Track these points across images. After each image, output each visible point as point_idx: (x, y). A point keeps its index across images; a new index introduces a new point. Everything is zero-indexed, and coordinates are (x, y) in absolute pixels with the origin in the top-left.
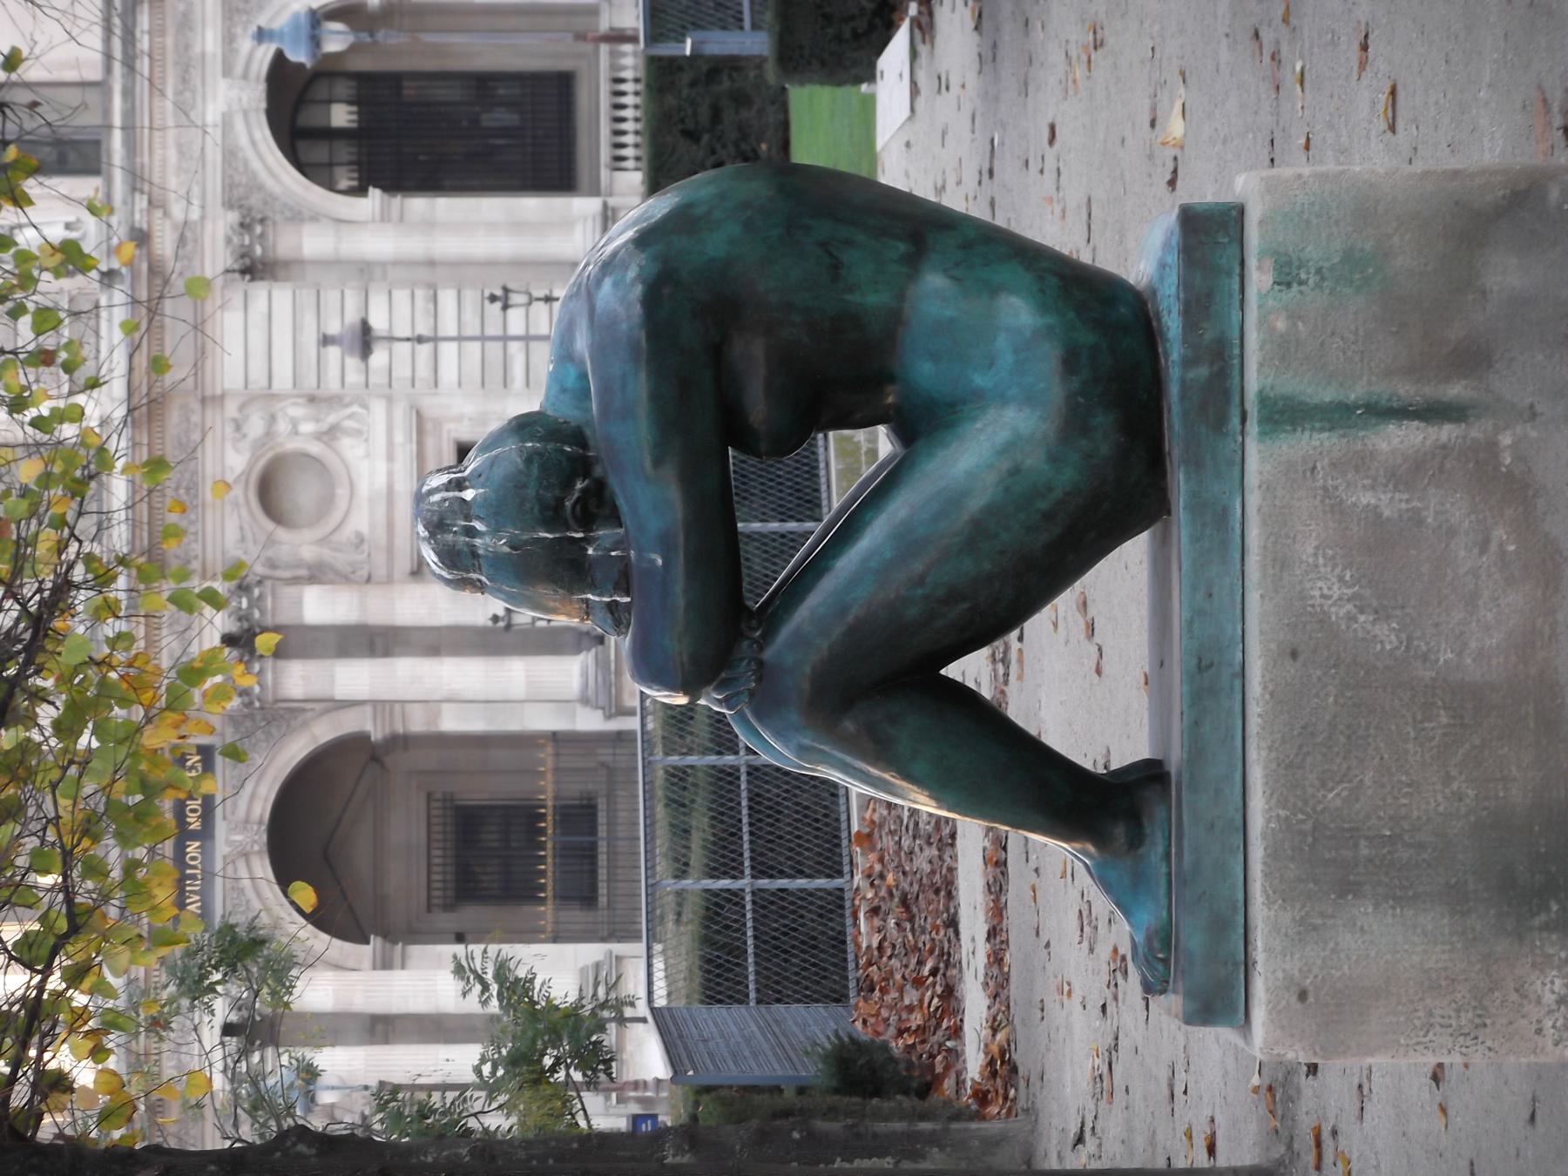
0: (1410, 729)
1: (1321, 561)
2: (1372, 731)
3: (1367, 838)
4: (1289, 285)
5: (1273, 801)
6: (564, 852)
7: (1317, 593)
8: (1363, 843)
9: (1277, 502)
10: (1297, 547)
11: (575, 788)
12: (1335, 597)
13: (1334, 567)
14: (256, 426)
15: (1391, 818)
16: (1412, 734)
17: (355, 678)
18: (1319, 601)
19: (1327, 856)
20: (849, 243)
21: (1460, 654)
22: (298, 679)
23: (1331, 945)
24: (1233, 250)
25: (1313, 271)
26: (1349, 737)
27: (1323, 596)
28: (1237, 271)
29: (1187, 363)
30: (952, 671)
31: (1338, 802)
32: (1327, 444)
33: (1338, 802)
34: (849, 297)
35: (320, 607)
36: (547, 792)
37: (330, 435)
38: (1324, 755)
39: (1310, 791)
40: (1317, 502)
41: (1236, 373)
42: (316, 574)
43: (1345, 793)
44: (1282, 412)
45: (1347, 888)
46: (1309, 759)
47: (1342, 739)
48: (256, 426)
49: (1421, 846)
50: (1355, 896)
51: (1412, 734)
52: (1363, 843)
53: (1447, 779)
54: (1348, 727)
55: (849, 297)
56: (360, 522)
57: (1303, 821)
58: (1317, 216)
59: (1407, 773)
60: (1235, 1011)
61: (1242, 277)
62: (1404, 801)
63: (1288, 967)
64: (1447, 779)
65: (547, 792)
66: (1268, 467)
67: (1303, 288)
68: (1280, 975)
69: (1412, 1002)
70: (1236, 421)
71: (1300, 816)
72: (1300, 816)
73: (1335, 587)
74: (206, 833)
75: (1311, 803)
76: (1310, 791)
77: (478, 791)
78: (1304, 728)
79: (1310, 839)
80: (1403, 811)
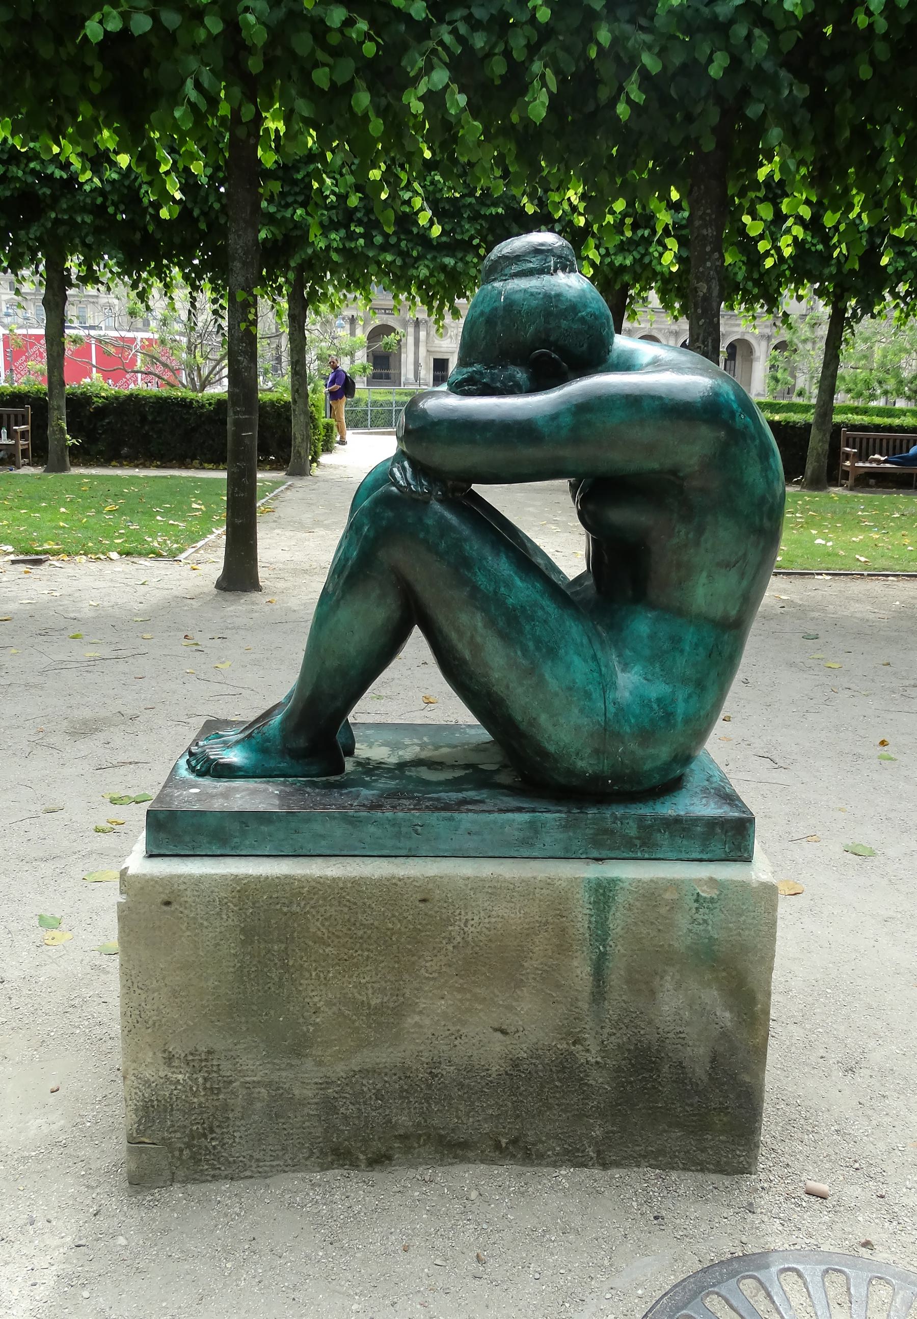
0: (367, 979)
1: (493, 920)
2: (366, 953)
3: (286, 948)
4: (696, 901)
5: (313, 884)
6: (381, 374)
7: (469, 917)
8: (283, 946)
9: (537, 890)
10: (505, 904)
11: (392, 376)
12: (466, 929)
13: (489, 929)
14: (453, 325)
15: (301, 966)
16: (363, 981)
17: (411, 340)
18: (464, 918)
19: (273, 921)
20: (742, 575)
21: (421, 1013)
22: (411, 330)
23: (205, 923)
24: (720, 853)
25: (706, 917)
26: (361, 938)
27: (467, 920)
28: (705, 857)
29: (641, 819)
30: (416, 631)
31: (313, 930)
32: (579, 925)
33: (313, 930)
34: (704, 574)
35: (423, 334)
36: (392, 371)
37: (451, 337)
38: (349, 920)
39: (322, 910)
40: (537, 918)
41: (631, 855)
42: (428, 334)
43: (319, 933)
44: (604, 894)
45: (248, 934)
46: (346, 910)
47: (360, 933)
48: (453, 325)
49: (281, 986)
50: (242, 941)
51: (363, 981)
52: (283, 946)
53: (330, 1004)
54: (369, 937)
55: (704, 574)
56: (436, 342)
57: (299, 905)
58: (744, 921)
59: (334, 977)
60: (158, 847)
61: (701, 860)
62: (314, 974)
63: (189, 893)
64: (330, 1004)
65: (392, 371)
66: (564, 885)
67: (694, 911)
68: (182, 887)
69: (164, 979)
70: (595, 854)
71: (303, 903)
72: (303, 903)
73: (472, 929)
74: (385, 313)
75: (314, 911)
76: (322, 910)
77: (391, 359)
78: (369, 906)
79: (285, 909)
80: (307, 975)
